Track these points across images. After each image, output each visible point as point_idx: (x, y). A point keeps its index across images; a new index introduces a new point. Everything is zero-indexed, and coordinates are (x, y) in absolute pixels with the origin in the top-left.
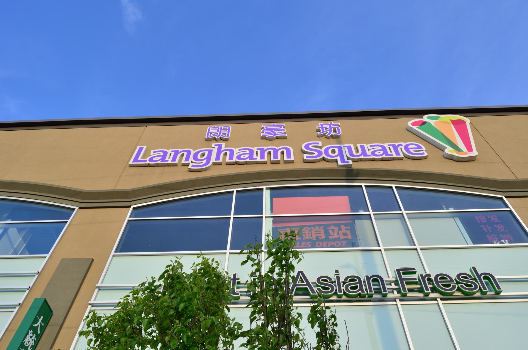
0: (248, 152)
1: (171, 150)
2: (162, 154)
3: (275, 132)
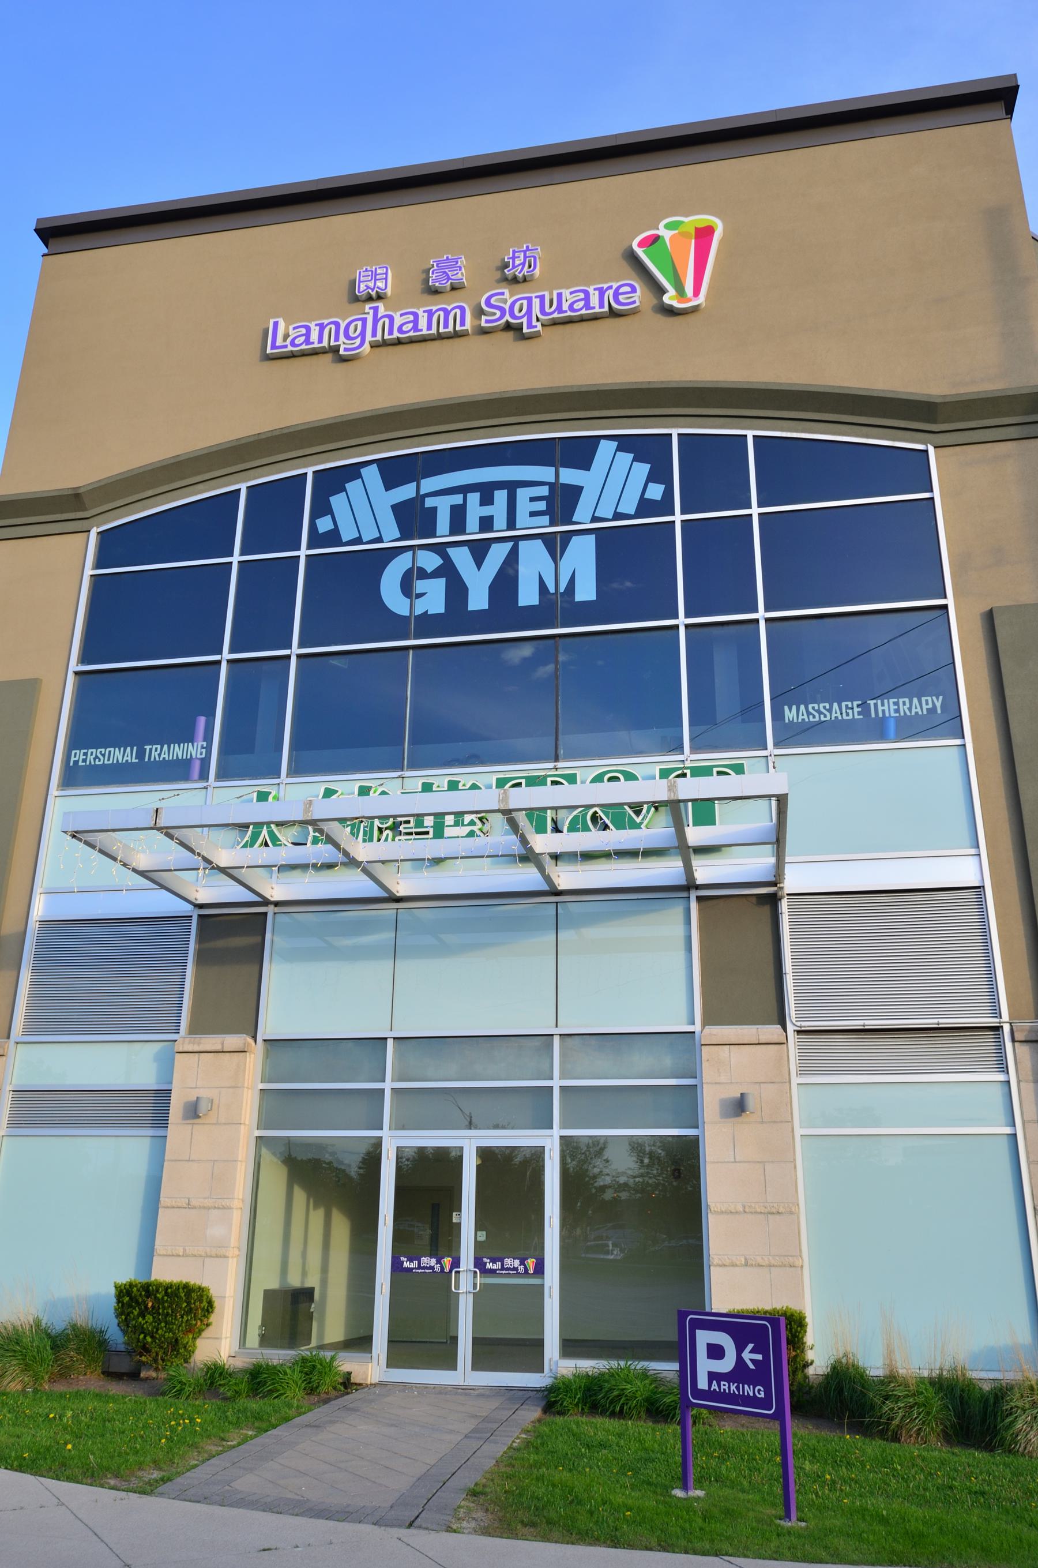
0: (582, 295)
1: (422, 310)
2: (304, 331)
3: (449, 273)
